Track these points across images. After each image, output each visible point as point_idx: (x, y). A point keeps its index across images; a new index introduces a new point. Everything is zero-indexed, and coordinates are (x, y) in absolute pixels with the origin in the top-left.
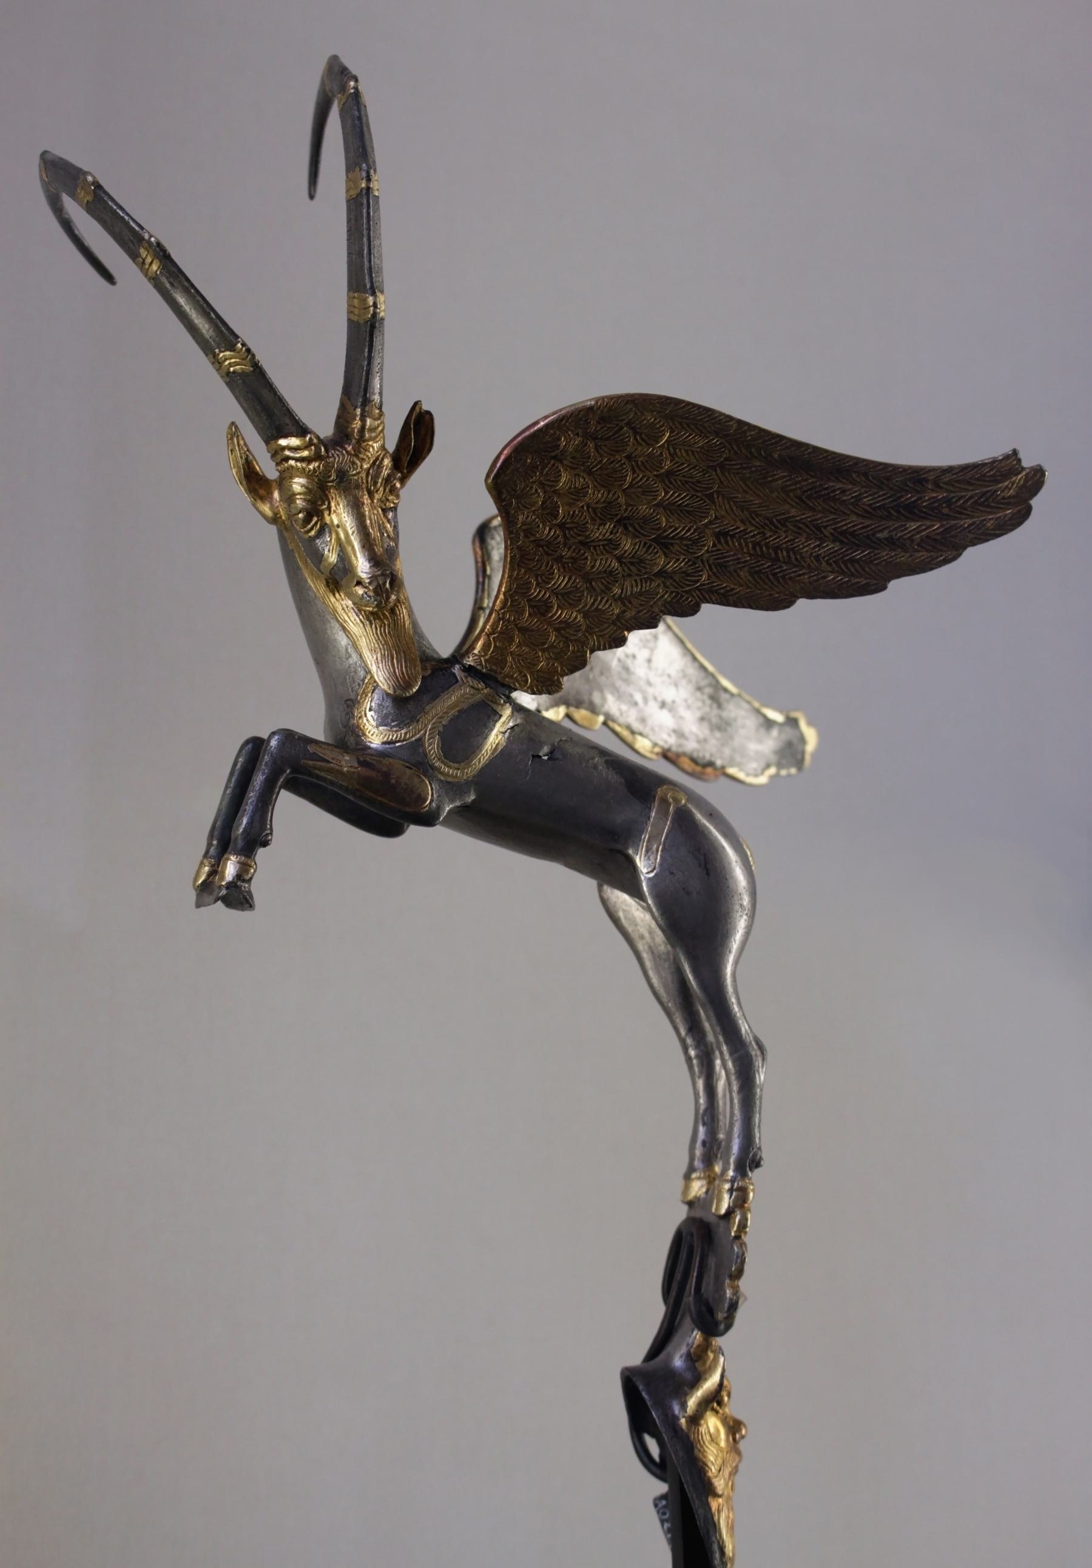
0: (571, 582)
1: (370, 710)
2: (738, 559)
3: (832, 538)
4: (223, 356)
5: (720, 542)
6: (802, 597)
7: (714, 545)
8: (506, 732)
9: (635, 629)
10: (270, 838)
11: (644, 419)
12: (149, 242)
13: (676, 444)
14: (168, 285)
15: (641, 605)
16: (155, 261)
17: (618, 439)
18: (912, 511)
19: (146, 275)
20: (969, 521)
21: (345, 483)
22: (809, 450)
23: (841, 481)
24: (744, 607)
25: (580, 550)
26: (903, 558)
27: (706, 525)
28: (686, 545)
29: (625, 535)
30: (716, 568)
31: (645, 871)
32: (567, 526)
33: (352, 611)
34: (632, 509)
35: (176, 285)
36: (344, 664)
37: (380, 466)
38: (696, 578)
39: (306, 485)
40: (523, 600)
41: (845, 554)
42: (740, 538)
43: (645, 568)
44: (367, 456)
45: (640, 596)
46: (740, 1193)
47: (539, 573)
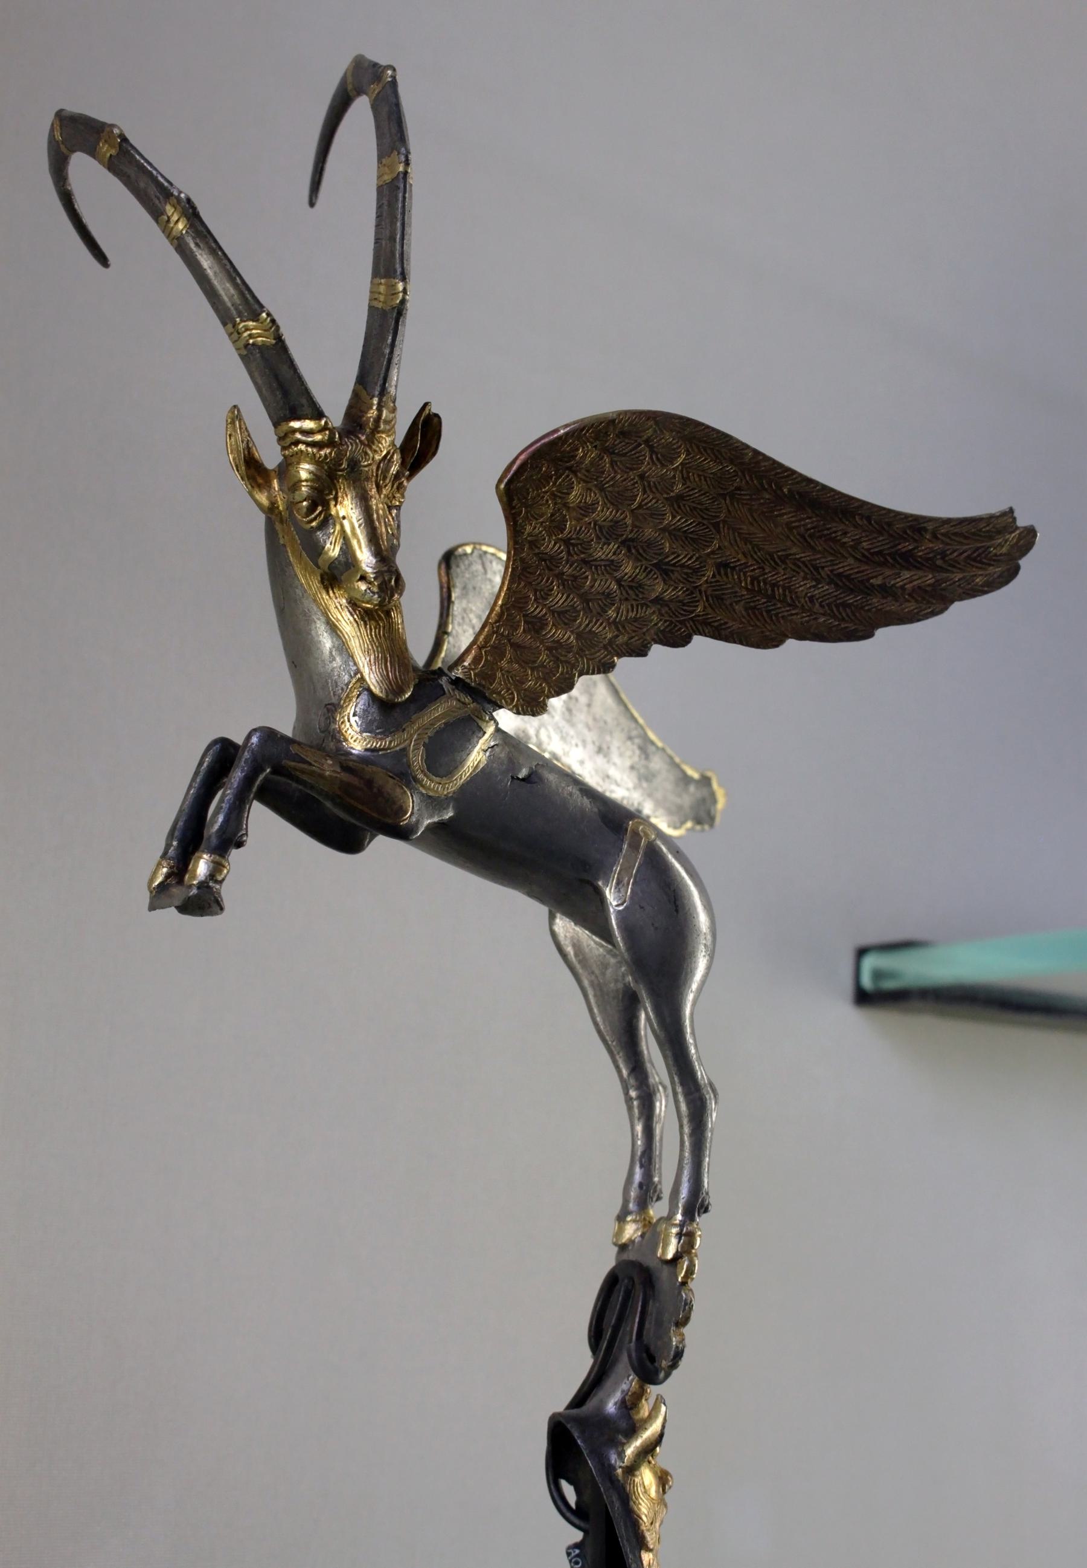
0: (569, 600)
1: (354, 715)
2: (736, 592)
3: (827, 580)
4: (243, 327)
5: (719, 574)
6: (791, 638)
7: (714, 576)
8: (487, 750)
9: (625, 656)
10: (245, 838)
11: (663, 438)
12: (178, 198)
13: (690, 467)
14: (192, 245)
15: (634, 631)
16: (181, 220)
17: (634, 456)
18: (908, 560)
19: (168, 237)
20: (960, 576)
21: (355, 475)
22: (818, 488)
23: (843, 523)
24: (735, 642)
25: (581, 569)
26: (893, 606)
27: (708, 555)
28: (686, 574)
29: (628, 557)
30: (713, 600)
31: (615, 903)
32: (572, 541)
33: (346, 610)
34: (638, 531)
35: (201, 245)
36: (327, 667)
37: (390, 461)
38: (691, 609)
39: (315, 471)
40: (520, 615)
41: (839, 597)
42: (740, 570)
43: (643, 593)
44: (380, 448)
45: (635, 621)
46: (687, 1238)
47: (539, 588)
